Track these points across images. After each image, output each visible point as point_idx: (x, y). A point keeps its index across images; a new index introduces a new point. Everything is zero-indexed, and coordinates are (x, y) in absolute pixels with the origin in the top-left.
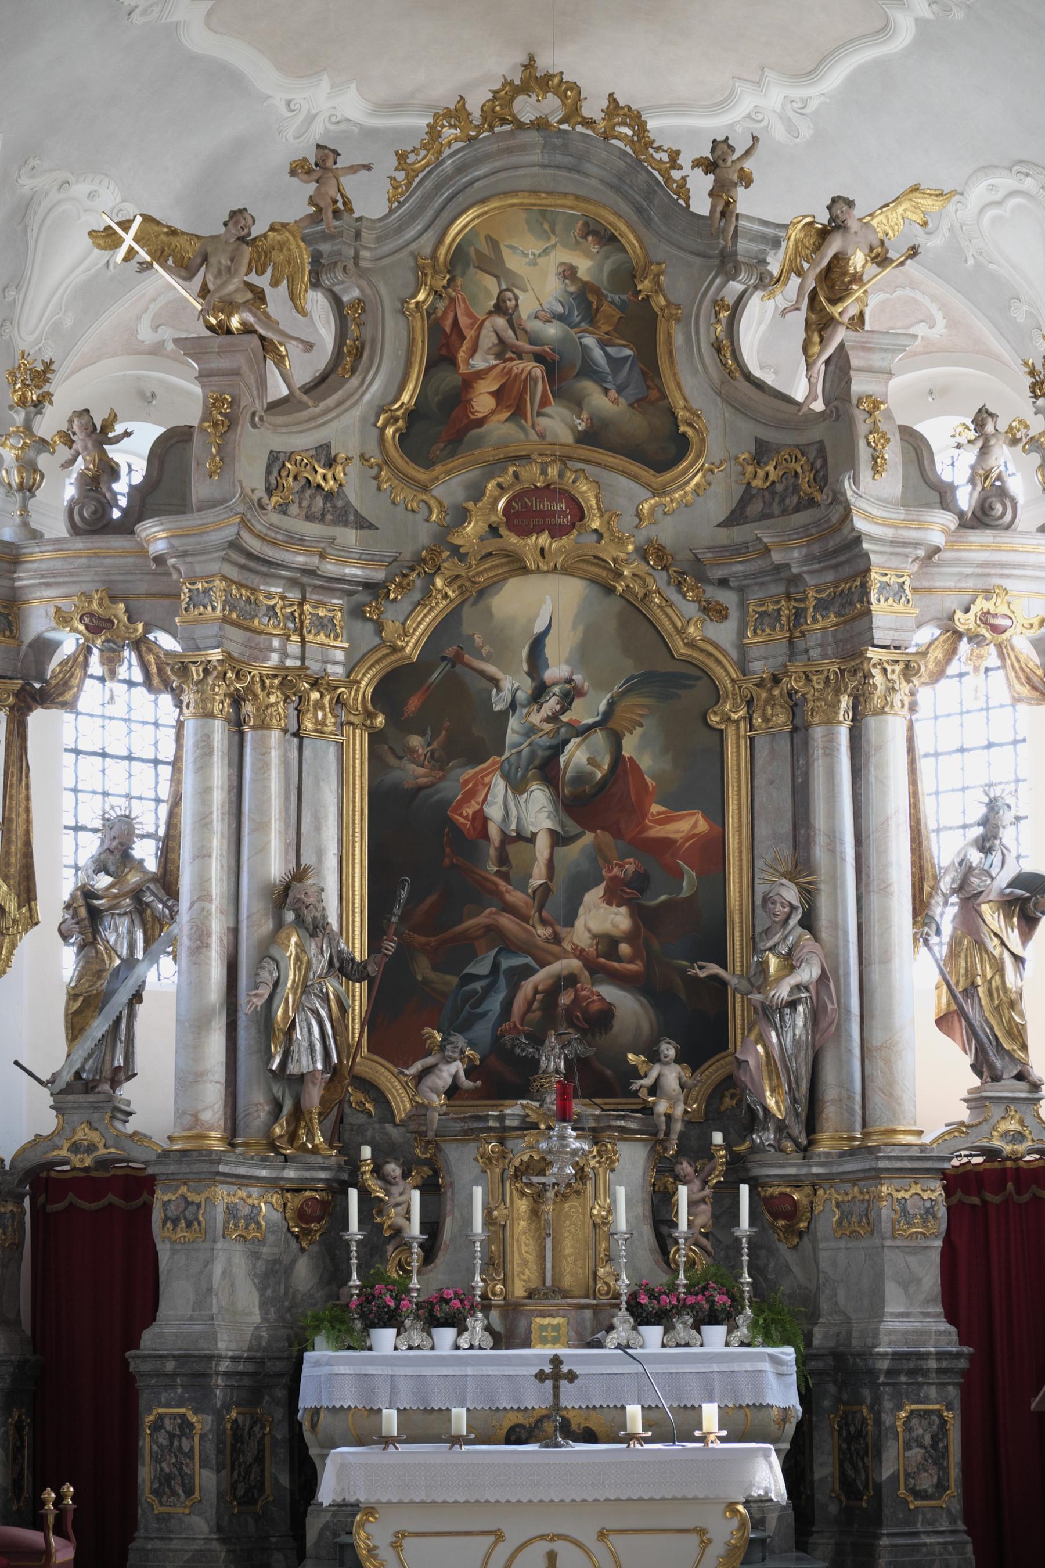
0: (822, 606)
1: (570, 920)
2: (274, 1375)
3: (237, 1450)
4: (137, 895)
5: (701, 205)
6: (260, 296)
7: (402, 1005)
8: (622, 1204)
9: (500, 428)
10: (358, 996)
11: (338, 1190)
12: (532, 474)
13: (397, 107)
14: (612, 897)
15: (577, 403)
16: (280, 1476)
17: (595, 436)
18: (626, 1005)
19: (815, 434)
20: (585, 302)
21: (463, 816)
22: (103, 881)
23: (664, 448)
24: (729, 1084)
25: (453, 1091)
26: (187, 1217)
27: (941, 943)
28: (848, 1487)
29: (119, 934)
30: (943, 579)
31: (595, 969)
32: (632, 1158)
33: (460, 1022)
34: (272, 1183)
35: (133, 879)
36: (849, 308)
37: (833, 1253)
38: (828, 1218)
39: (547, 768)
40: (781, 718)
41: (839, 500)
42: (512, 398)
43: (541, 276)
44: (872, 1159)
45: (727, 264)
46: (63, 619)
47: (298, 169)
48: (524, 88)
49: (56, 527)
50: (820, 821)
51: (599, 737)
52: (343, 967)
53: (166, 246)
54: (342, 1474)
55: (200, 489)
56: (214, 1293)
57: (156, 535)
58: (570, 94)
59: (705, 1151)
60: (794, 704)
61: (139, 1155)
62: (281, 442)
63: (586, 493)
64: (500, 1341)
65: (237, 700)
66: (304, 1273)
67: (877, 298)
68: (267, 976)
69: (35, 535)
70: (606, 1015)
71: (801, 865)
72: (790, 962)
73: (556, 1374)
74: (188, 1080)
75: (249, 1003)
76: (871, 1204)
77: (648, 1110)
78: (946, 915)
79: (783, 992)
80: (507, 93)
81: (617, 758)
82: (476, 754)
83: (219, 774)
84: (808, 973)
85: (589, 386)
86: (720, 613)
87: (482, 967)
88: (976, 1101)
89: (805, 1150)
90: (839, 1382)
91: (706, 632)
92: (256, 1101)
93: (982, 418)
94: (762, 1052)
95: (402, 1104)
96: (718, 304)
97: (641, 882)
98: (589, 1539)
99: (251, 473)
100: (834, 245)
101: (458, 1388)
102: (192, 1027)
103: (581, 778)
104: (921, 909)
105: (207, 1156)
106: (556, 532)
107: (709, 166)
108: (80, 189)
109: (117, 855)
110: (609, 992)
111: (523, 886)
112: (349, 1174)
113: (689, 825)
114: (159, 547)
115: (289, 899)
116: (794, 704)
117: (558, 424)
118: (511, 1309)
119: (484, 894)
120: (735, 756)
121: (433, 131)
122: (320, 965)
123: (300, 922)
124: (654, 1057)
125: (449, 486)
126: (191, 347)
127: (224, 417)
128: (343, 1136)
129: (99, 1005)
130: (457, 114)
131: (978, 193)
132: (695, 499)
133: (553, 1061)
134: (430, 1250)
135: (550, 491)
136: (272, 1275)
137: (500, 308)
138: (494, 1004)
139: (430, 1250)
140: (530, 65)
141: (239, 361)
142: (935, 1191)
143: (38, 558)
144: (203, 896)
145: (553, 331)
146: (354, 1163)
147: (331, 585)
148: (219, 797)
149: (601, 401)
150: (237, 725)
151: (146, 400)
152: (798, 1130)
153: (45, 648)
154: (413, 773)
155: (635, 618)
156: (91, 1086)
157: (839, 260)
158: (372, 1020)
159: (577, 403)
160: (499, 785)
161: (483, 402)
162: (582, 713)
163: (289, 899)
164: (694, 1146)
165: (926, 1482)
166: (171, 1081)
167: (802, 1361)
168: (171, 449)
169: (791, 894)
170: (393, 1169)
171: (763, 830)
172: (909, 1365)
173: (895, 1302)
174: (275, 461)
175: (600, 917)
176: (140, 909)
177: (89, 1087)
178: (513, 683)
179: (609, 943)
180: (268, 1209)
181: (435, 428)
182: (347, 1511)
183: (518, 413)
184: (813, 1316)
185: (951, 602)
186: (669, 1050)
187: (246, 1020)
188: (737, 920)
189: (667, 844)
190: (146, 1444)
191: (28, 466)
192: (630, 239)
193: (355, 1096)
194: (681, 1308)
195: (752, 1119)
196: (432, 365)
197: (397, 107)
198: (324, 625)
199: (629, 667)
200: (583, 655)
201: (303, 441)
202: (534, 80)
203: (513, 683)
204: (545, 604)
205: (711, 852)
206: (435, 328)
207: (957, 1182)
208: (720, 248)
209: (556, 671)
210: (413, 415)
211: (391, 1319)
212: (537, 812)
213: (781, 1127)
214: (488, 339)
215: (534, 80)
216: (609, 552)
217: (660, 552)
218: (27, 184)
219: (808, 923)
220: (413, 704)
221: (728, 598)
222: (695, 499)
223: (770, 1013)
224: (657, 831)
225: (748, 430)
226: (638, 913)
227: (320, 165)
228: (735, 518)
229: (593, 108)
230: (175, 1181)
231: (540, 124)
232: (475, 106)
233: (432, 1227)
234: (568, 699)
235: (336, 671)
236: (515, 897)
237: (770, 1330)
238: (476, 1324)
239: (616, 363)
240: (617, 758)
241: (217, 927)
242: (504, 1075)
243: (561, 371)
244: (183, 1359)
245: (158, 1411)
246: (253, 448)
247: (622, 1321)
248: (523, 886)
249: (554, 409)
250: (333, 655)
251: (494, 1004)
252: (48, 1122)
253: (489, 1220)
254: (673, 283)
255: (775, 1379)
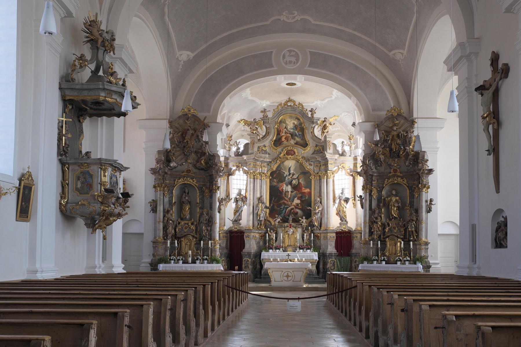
0: (323, 165)
1: (293, 202)
2: (258, 255)
3: (254, 263)
4: (242, 199)
5: (310, 116)
6: (257, 128)
7: (273, 211)
8: (298, 236)
9: (285, 142)
10: (268, 210)
11: (265, 233)
12: (289, 148)
13: (273, 103)
14: (298, 199)
15: (295, 139)
16: (258, 266)
17: (296, 144)
18: (300, 212)
19: (323, 144)
20: (296, 127)
21: (280, 189)
22: (238, 197)
23: (305, 145)
24: (311, 221)
25: (279, 222)
26: (248, 237)
27: (336, 205)
28: (324, 268)
29: (240, 203)
30: (338, 162)
31: (296, 208)
32: (300, 230)
33: (279, 214)
34: (258, 233)
35: (242, 196)
36: (327, 130)
37: (322, 242)
38: (322, 238)
39: (290, 183)
40: (318, 178)
41: (324, 153)
42: (287, 139)
43: (291, 124)
44: (327, 231)
45: (313, 123)
46: (234, 166)
47: (262, 112)
48: (289, 101)
49: (233, 155)
50: (322, 191)
51: (297, 180)
52: (266, 207)
53: (246, 123)
54: (266, 265)
55: (250, 151)
56: (251, 245)
57: (245, 157)
58: (294, 102)
59: (308, 229)
60: (320, 176)
61: (242, 229)
62: (259, 145)
63: (295, 150)
64: (284, 251)
65: (254, 176)
66: (261, 243)
67: (330, 128)
68: (257, 209)
69: (230, 156)
70: (297, 213)
71: (320, 196)
72: (318, 208)
73: (288, 255)
74: (248, 221)
75: (255, 212)
76: (327, 236)
77: (301, 225)
78: (337, 201)
79: (317, 211)
80: (287, 102)
81: (299, 182)
82: (282, 182)
83: (252, 185)
84: (320, 209)
85: (296, 137)
86: (312, 165)
87: (283, 207)
88: (340, 224)
89: (320, 230)
90: (323, 256)
91: (309, 167)
92: (256, 223)
93: (343, 142)
94: (315, 219)
95: (273, 223)
96: (312, 127)
97: (301, 197)
98: (291, 271)
99: (256, 149)
100: (325, 123)
101: (279, 256)
102: (249, 215)
103: (295, 184)
104: (334, 201)
105: (250, 229)
106: (292, 155)
107: (311, 111)
108: (236, 114)
109: (239, 194)
110: (297, 210)
111: (287, 197)
112: (267, 232)
113: (307, 190)
114: (245, 158)
115: (260, 199)
116: (320, 176)
117: (292, 142)
118: (285, 248)
119: (283, 198)
120: (313, 182)
121: (278, 107)
122: (264, 207)
123: (261, 202)
124: (302, 218)
125: (279, 149)
126: (249, 135)
127: (253, 143)
128: (266, 227)
129: (238, 211)
130: (280, 104)
131: (343, 114)
132: (309, 151)
133: (291, 218)
134: (276, 241)
135: (292, 150)
136: (258, 243)
137: (285, 128)
138: (284, 211)
139: (276, 241)
140: (289, 98)
141: (255, 136)
142: (334, 235)
143: (231, 159)
144: (250, 199)
145: (292, 130)
146: (267, 230)
147: (265, 162)
148: (252, 188)
149: (297, 139)
150: (254, 178)
151: (242, 136)
152: (319, 227)
153: (231, 169)
154: (275, 184)
155: (301, 165)
156: (236, 221)
157: (325, 125)
158: (269, 214)
159: (295, 139)
160: (285, 185)
161: (283, 139)
162: (295, 177)
163: (260, 199)
164: (307, 229)
165: (332, 268)
166: (246, 220)
167: (319, 254)
168: (246, 145)
169: (319, 199)
170: (272, 231)
171: (316, 191)
172: (331, 255)
173: (329, 247)
174: (259, 147)
175: (297, 201)
176: (242, 200)
177: (236, 221)
178: (287, 173)
179: (297, 204)
180: (257, 236)
181: (278, 142)
182: (267, 270)
183: (287, 141)
184: (320, 249)
185: (339, 164)
186: (304, 218)
187: (255, 214)
188: (151, 320)
189: (305, 192)
190: (243, 262)
191: (230, 148)
192: (301, 120)
193: (267, 222)
194: (305, 248)
195: (313, 226)
196: (277, 135)
197: (273, 103)
198: (264, 166)
199: (300, 171)
200: (295, 170)
201: (262, 144)
202: (290, 100)
203: (287, 173)
204: (290, 163)
205: (310, 193)
206: (278, 130)
207: (337, 233)
208: (312, 121)
209: (292, 172)
210: (275, 141)
211: (272, 249)
212: (289, 188)
213: (317, 227)
214: (284, 132)
215: (290, 100)
216: (298, 158)
217: (304, 158)
218: (230, 114)
219: (321, 203)
220: (275, 176)
221: (312, 163)
222: (309, 151)
223: (315, 213)
224: (303, 191)
225: (315, 143)
226: (301, 201)
227: (264, 111)
228: (313, 154)
229: (297, 103)
230: (247, 233)
231: (291, 106)
232: (283, 102)
233: (276, 238)
234: (293, 175)
235: (266, 172)
236: (286, 199)
237: (315, 251)
238: (281, 249)
239: (299, 134)
240: (299, 182)
241: (252, 203)
242: (285, 220)
243: (293, 135)
244: (248, 253)
245: (245, 259)
246: (256, 146)
247: (298, 249)
248: (287, 197)
249: (292, 140)
250: (265, 170)
251: (284, 211)
252: (232, 225)
253: (283, 237)
254: (306, 125)
255: (315, 256)
